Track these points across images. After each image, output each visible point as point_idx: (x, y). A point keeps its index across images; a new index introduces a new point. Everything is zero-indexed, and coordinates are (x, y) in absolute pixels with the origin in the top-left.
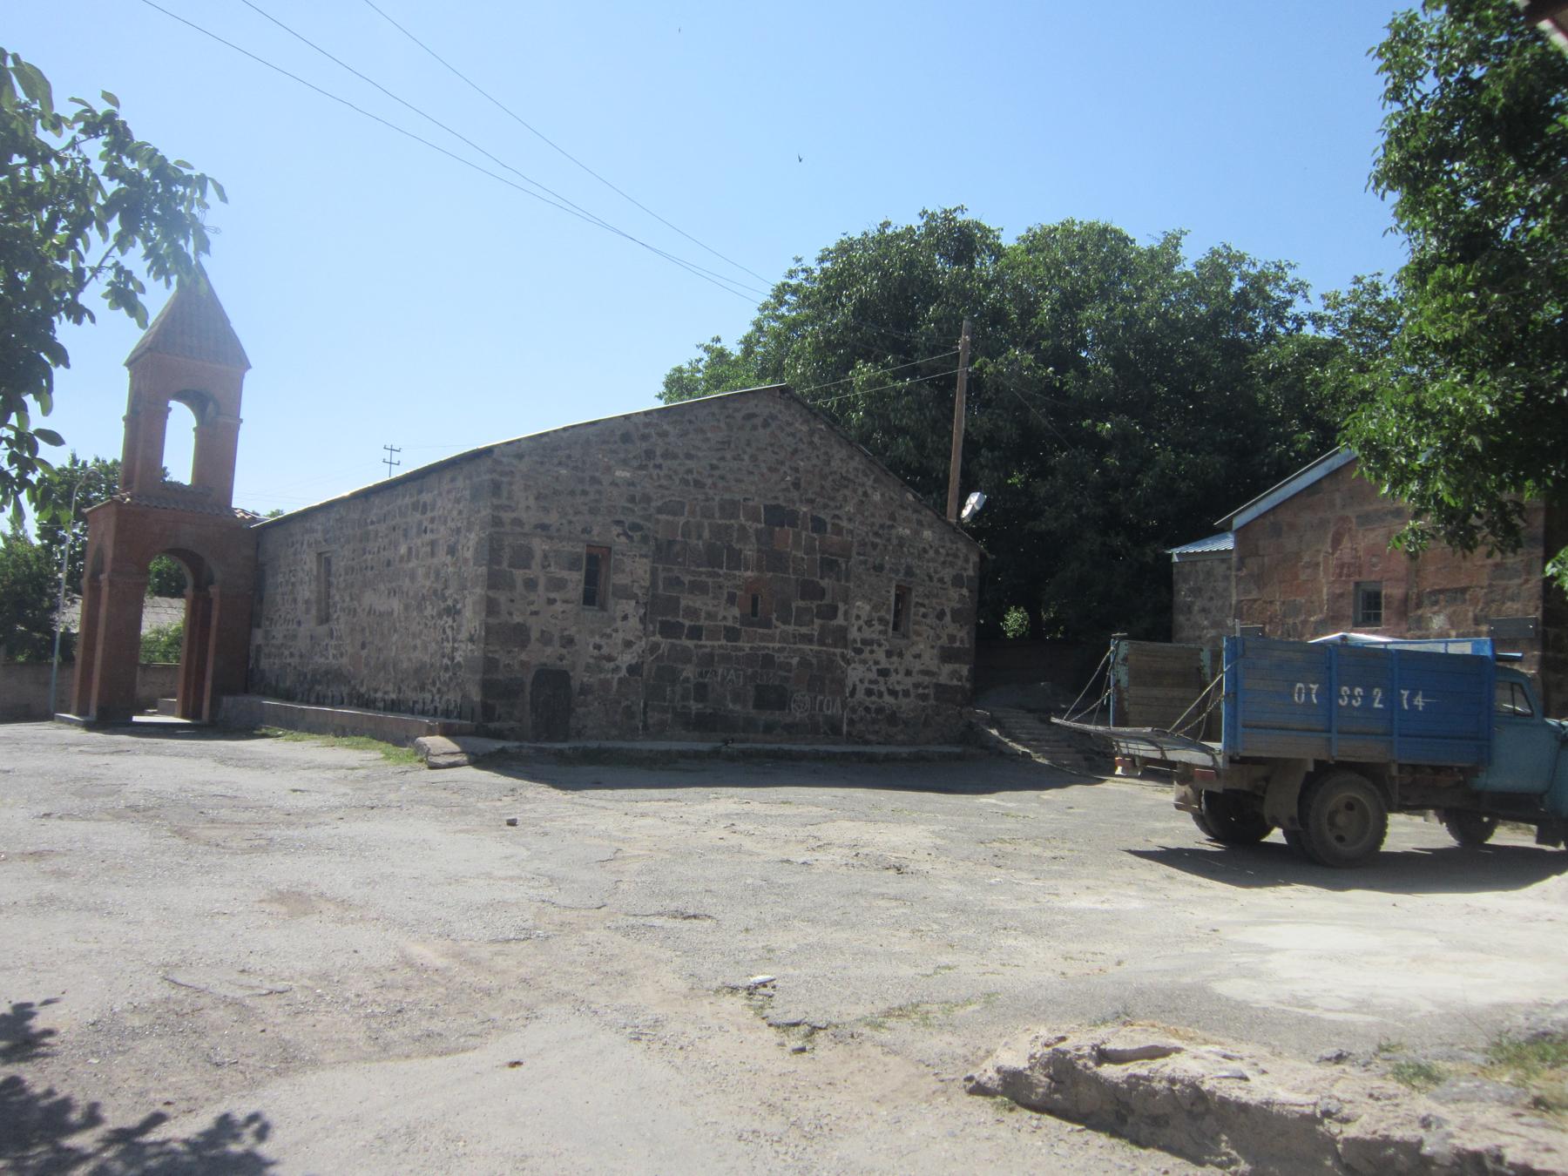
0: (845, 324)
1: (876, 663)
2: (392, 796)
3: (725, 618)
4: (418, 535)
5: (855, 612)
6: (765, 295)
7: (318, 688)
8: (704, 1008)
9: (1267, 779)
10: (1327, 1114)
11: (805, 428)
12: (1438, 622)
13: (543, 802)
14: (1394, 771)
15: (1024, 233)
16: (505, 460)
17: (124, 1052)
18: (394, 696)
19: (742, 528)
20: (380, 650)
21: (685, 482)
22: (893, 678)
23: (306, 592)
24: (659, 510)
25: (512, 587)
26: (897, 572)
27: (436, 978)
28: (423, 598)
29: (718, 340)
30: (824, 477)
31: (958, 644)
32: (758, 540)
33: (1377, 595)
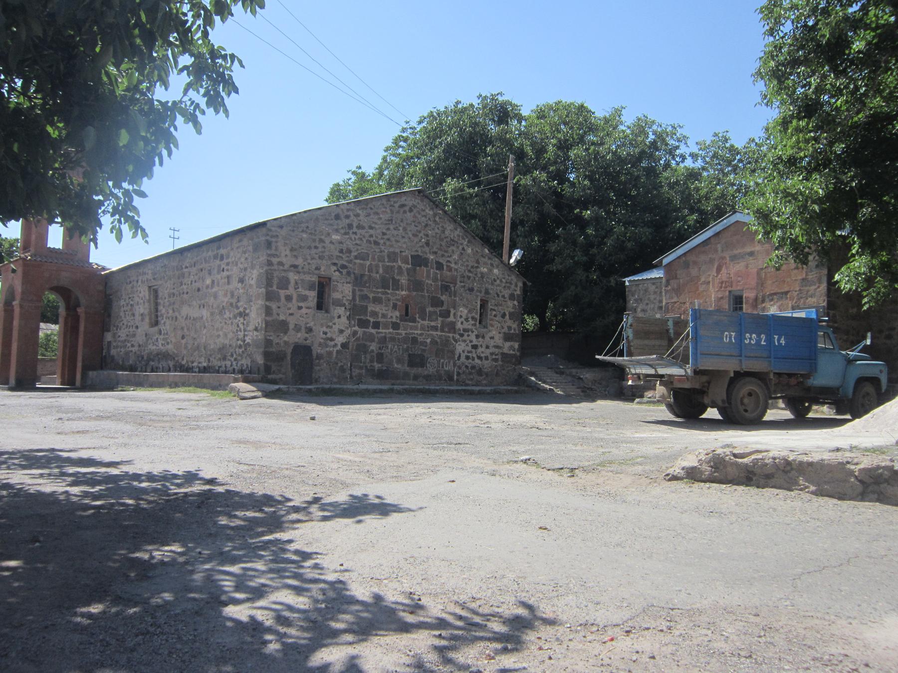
0: (438, 157)
1: (471, 342)
4: (218, 273)
7: (152, 363)
9: (709, 383)
10: (848, 463)
11: (431, 213)
14: (772, 376)
16: (273, 229)
18: (205, 364)
19: (400, 267)
21: (369, 242)
22: (480, 350)
23: (142, 309)
24: (356, 258)
25: (279, 300)
26: (480, 292)
29: (360, 168)
30: (442, 240)
31: (512, 331)
32: (408, 274)
33: (741, 297)
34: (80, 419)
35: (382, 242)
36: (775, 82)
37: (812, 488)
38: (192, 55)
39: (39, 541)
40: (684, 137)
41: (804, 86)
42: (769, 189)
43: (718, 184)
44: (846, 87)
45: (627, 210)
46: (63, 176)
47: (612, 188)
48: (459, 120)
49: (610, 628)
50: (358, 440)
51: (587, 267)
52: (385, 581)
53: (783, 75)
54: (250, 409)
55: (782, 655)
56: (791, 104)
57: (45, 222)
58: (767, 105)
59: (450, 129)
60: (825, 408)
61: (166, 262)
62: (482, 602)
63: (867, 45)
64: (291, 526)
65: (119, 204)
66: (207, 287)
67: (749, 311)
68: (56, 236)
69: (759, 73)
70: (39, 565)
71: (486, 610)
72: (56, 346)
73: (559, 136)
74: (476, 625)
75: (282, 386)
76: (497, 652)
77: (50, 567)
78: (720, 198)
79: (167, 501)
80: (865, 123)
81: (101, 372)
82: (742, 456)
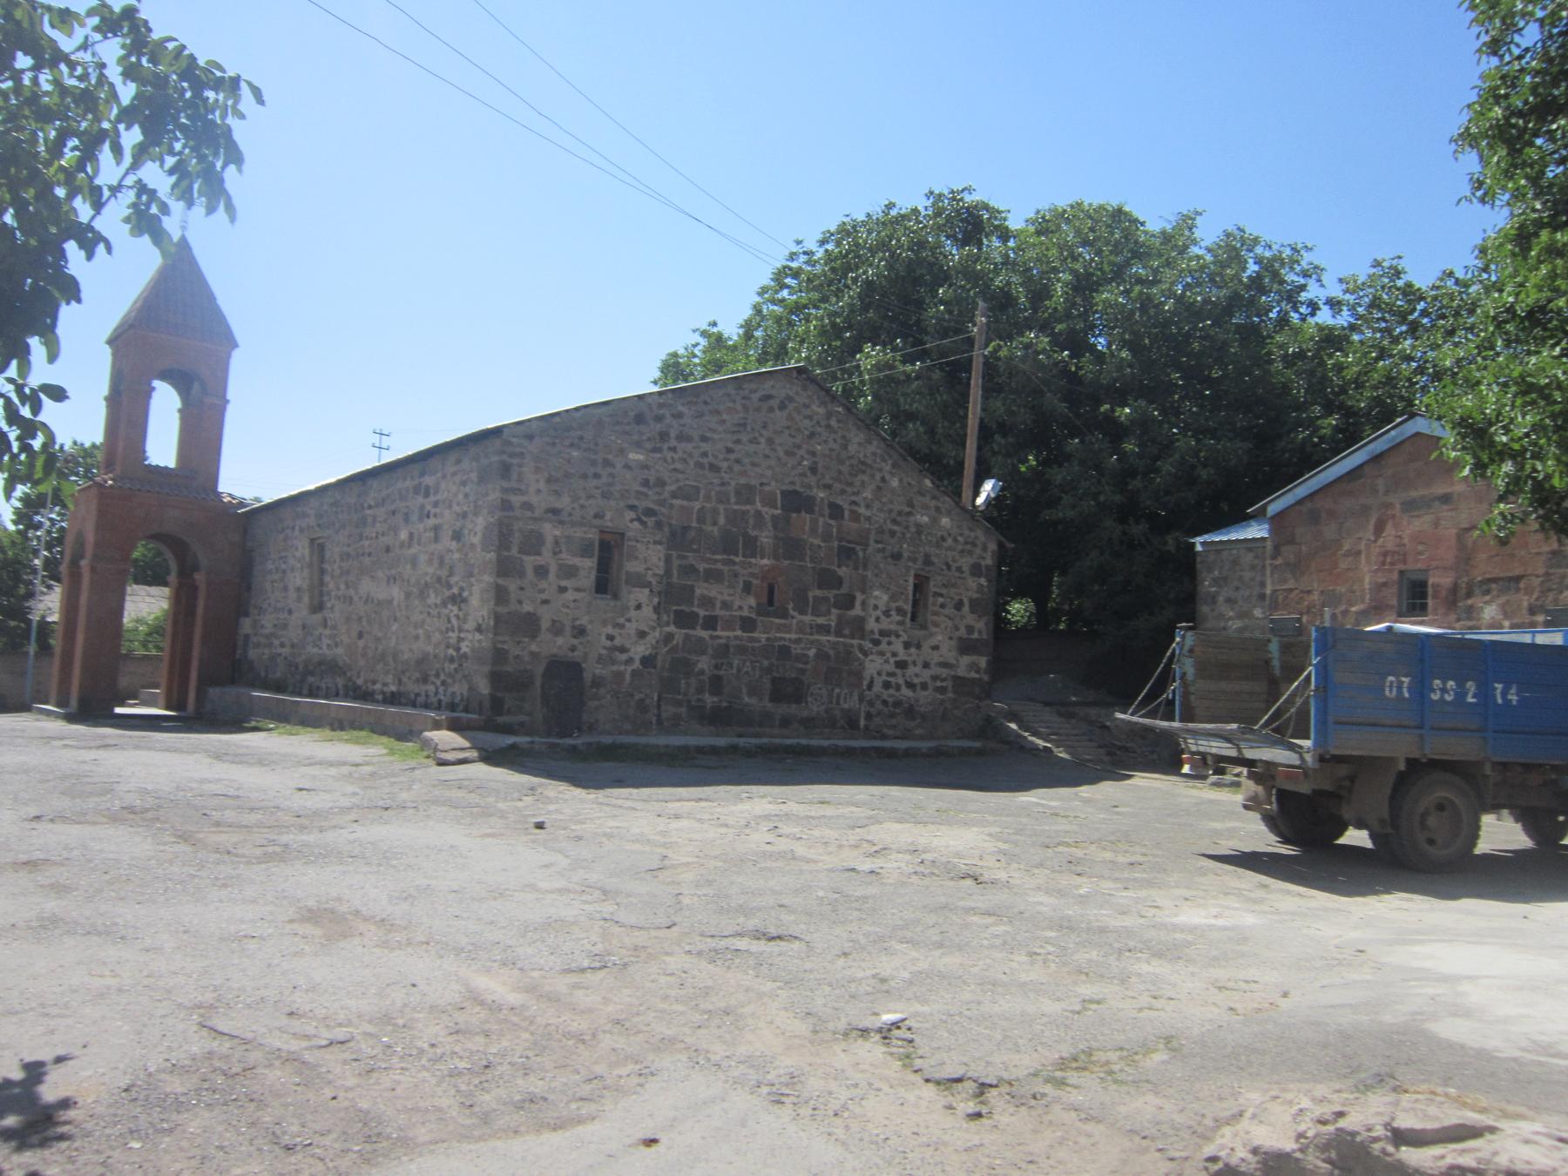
1: (894, 655)
2: (404, 795)
3: (741, 608)
4: (421, 519)
6: (765, 279)
7: (311, 679)
8: (840, 1056)
11: (821, 411)
12: (1490, 612)
13: (565, 801)
14: (1488, 770)
15: (1032, 215)
16: (514, 440)
17: (171, 1131)
18: (393, 688)
19: (758, 514)
20: (378, 640)
22: (911, 670)
23: (298, 579)
24: (674, 495)
25: (522, 574)
26: (915, 560)
27: (515, 1019)
28: (426, 584)
29: (715, 324)
30: (841, 462)
31: (975, 636)
32: (775, 527)
35: (725, 465)
40: (1316, 267)
43: (1380, 358)
45: (1201, 407)
47: (1178, 367)
48: (891, 238)
56: (1536, 196)
58: (1482, 201)
66: (402, 545)
78: (1385, 384)
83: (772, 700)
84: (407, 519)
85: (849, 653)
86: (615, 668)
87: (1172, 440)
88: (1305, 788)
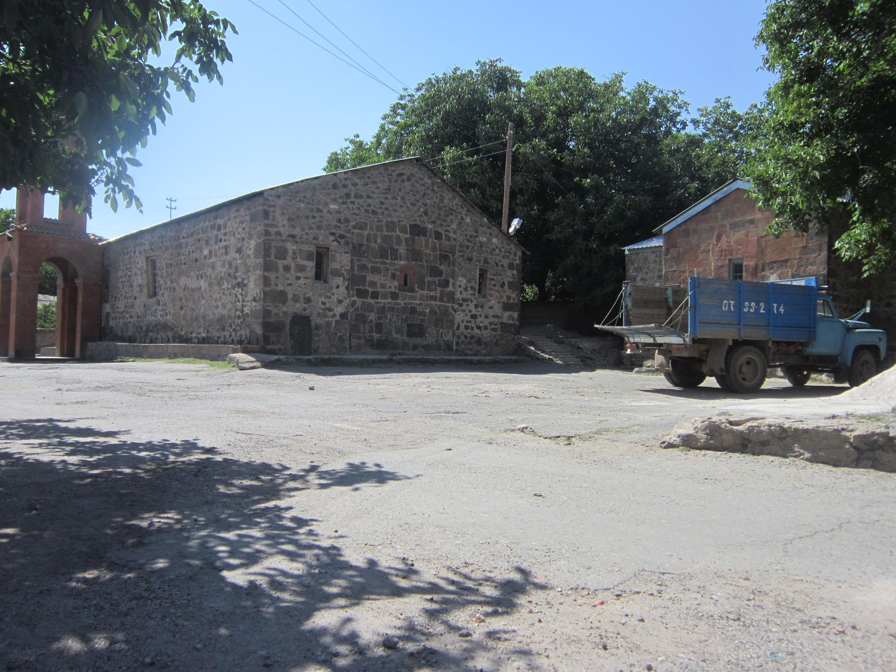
0: (437, 125)
1: (470, 311)
4: (216, 243)
5: (458, 283)
7: (151, 334)
9: (707, 351)
10: (843, 429)
11: (429, 181)
14: (770, 344)
15: (534, 74)
18: (204, 335)
19: (398, 237)
22: (479, 319)
23: (140, 280)
24: (354, 227)
25: (277, 270)
26: (479, 261)
29: (358, 136)
30: (440, 209)
31: (512, 301)
32: (406, 243)
33: (741, 266)
34: (79, 389)
35: (380, 211)
36: (777, 46)
37: (807, 455)
38: (183, 20)
39: (36, 509)
41: (807, 50)
42: (769, 156)
44: (849, 50)
46: (55, 144)
47: (612, 155)
48: (458, 87)
49: (600, 592)
50: (356, 409)
51: (587, 236)
52: (380, 547)
53: (785, 39)
54: (249, 379)
55: (771, 618)
56: (793, 68)
57: (39, 192)
58: (769, 69)
59: (449, 96)
60: (824, 377)
61: (163, 232)
62: (475, 567)
63: (871, 7)
64: (287, 494)
65: (112, 173)
66: (205, 257)
67: (749, 279)
68: (51, 206)
69: (761, 36)
70: (35, 532)
71: (478, 575)
72: (54, 318)
73: (559, 102)
74: (468, 589)
75: (281, 357)
76: (487, 615)
77: (46, 535)
79: (165, 469)
80: (868, 88)
81: (100, 343)
82: (738, 423)
83: (408, 336)
84: (207, 243)
85: (446, 311)
86: (326, 319)
87: (612, 195)
88: (685, 354)
